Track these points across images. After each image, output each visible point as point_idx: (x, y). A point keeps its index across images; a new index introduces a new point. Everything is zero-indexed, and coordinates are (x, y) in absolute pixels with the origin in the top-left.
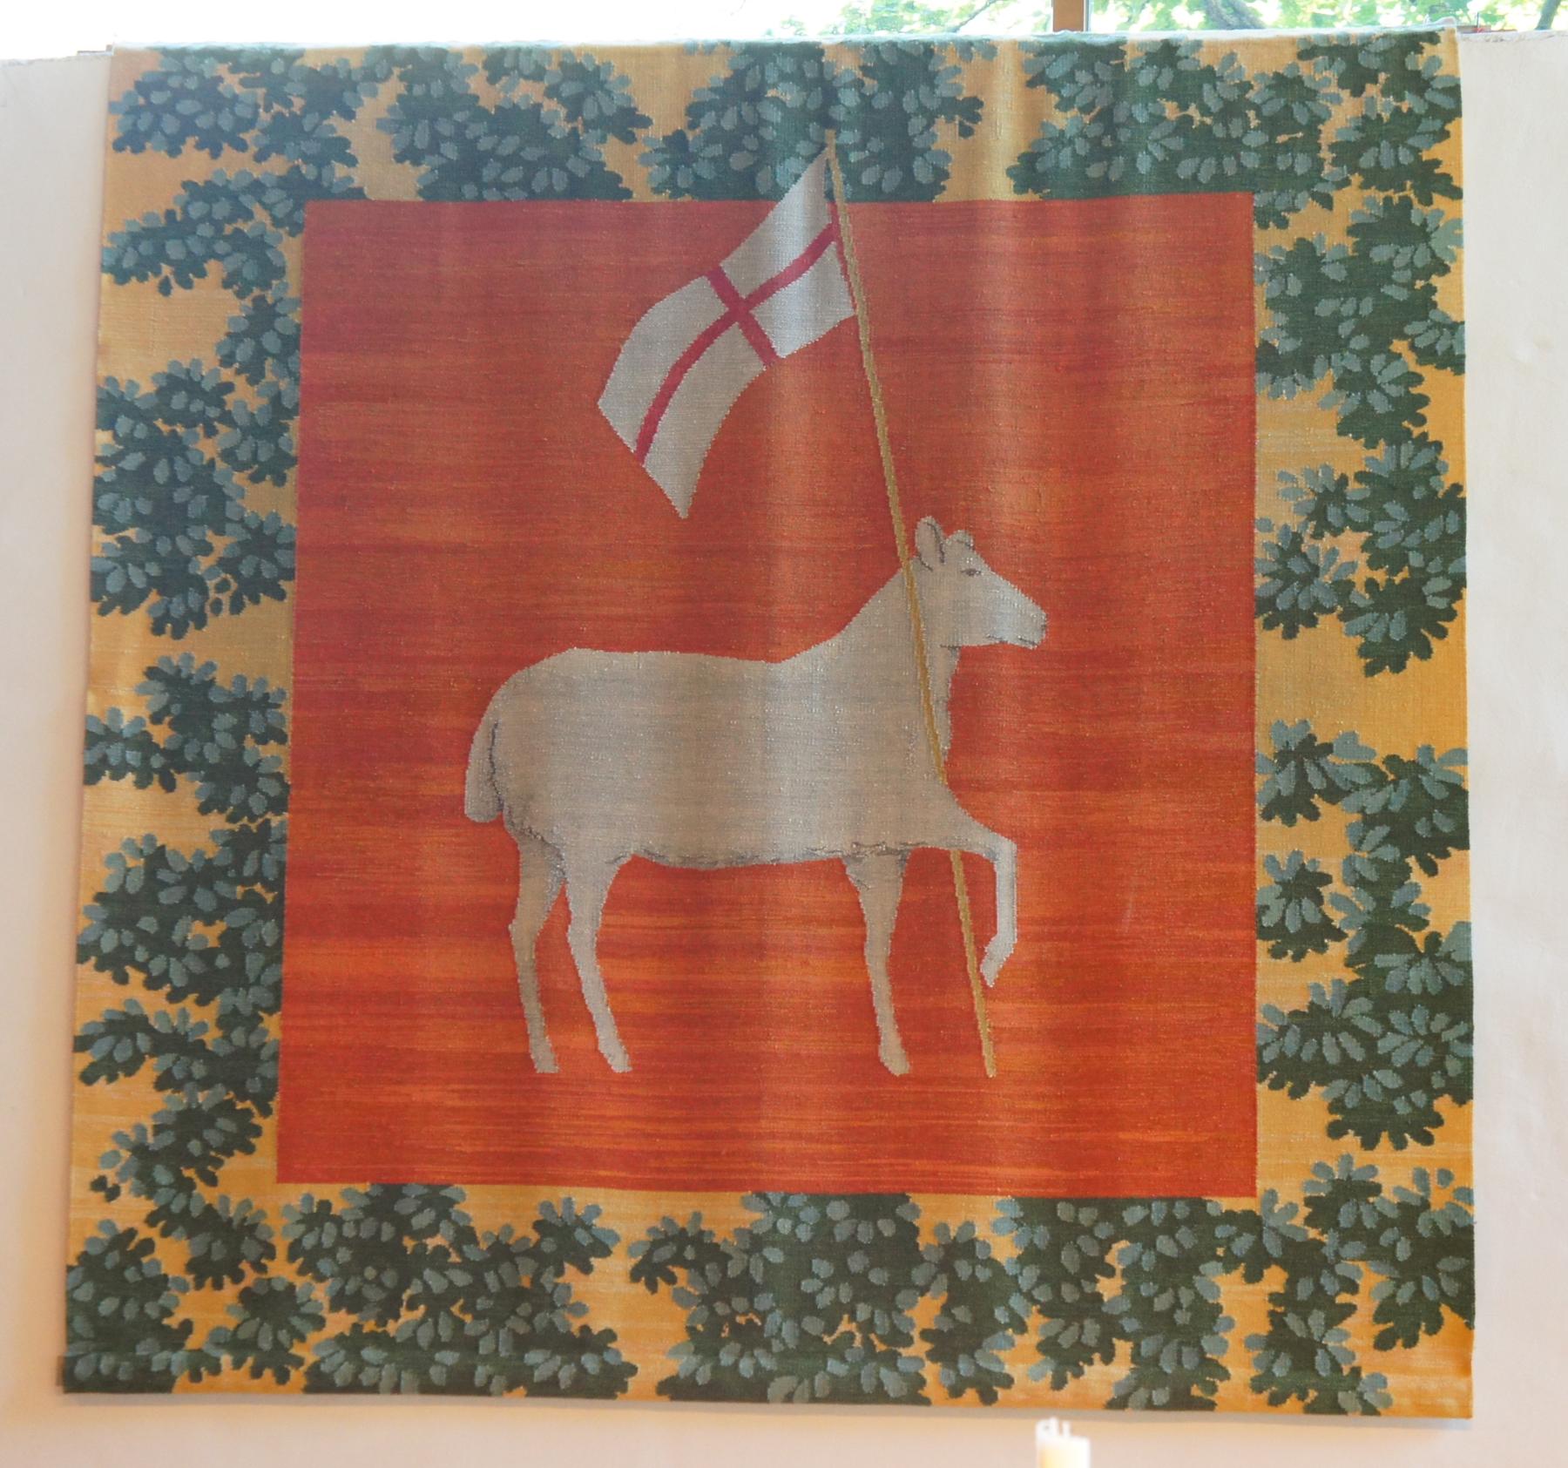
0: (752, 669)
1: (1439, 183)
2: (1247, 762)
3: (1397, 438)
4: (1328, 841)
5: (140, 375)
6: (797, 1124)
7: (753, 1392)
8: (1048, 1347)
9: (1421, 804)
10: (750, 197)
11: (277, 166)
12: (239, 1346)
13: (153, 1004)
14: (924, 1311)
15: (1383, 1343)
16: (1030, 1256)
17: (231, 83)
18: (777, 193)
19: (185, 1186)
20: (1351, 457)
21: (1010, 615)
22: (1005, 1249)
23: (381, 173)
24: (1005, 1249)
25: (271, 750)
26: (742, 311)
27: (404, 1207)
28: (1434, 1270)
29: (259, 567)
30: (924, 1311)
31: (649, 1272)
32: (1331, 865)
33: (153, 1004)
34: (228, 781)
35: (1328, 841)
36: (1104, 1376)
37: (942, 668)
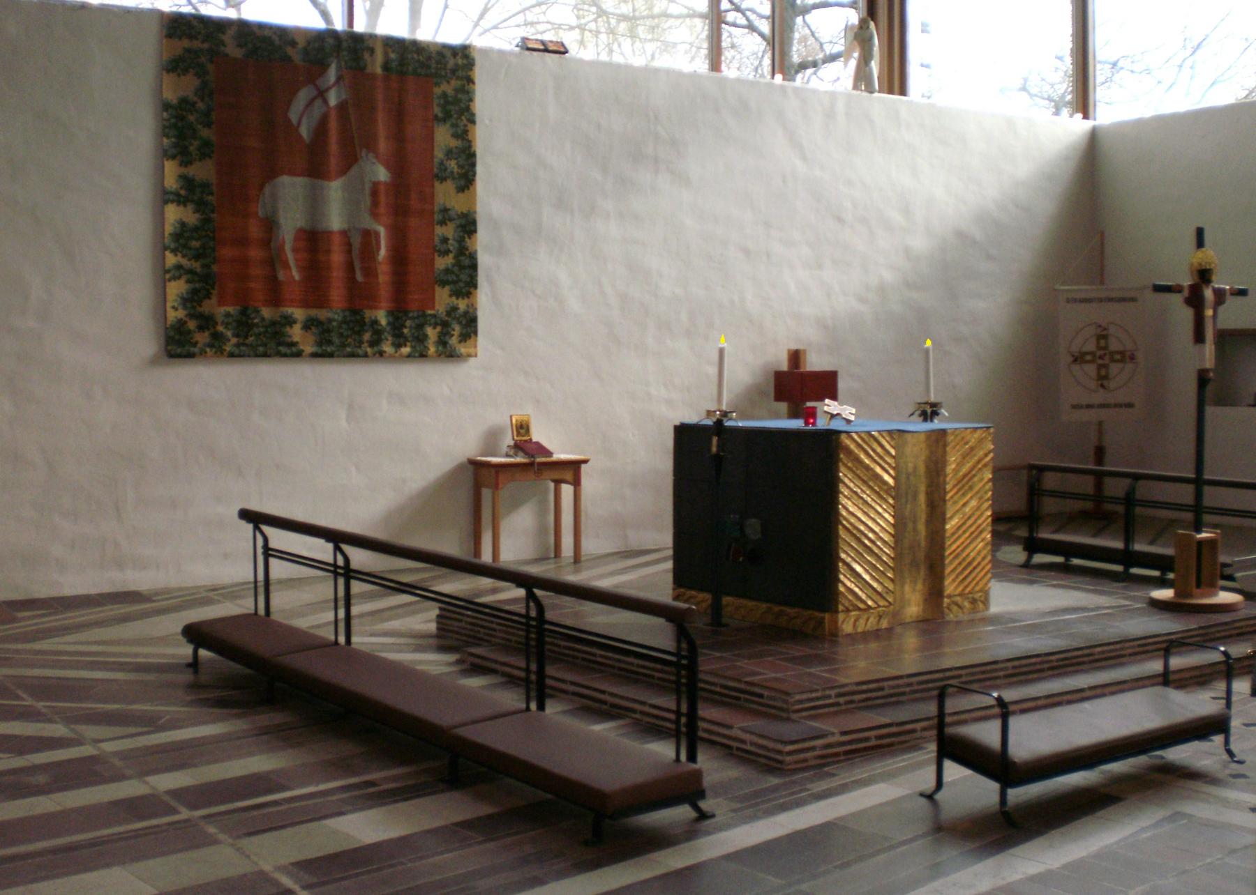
0: (326, 183)
1: (471, 81)
2: (432, 213)
3: (463, 139)
4: (449, 231)
5: (170, 96)
6: (337, 293)
7: (331, 355)
8: (393, 344)
9: (180, 343)
10: (323, 67)
11: (206, 46)
12: (211, 346)
13: (184, 262)
14: (367, 336)
15: (460, 342)
16: (389, 323)
17: (195, 23)
18: (329, 65)
19: (194, 307)
20: (454, 143)
21: (382, 174)
22: (384, 322)
23: (233, 50)
24: (384, 322)
25: (210, 198)
26: (322, 94)
27: (249, 312)
28: (469, 325)
29: (206, 150)
30: (367, 336)
31: (306, 327)
32: (450, 236)
33: (184, 262)
34: (201, 206)
35: (449, 231)
36: (406, 350)
37: (368, 186)
